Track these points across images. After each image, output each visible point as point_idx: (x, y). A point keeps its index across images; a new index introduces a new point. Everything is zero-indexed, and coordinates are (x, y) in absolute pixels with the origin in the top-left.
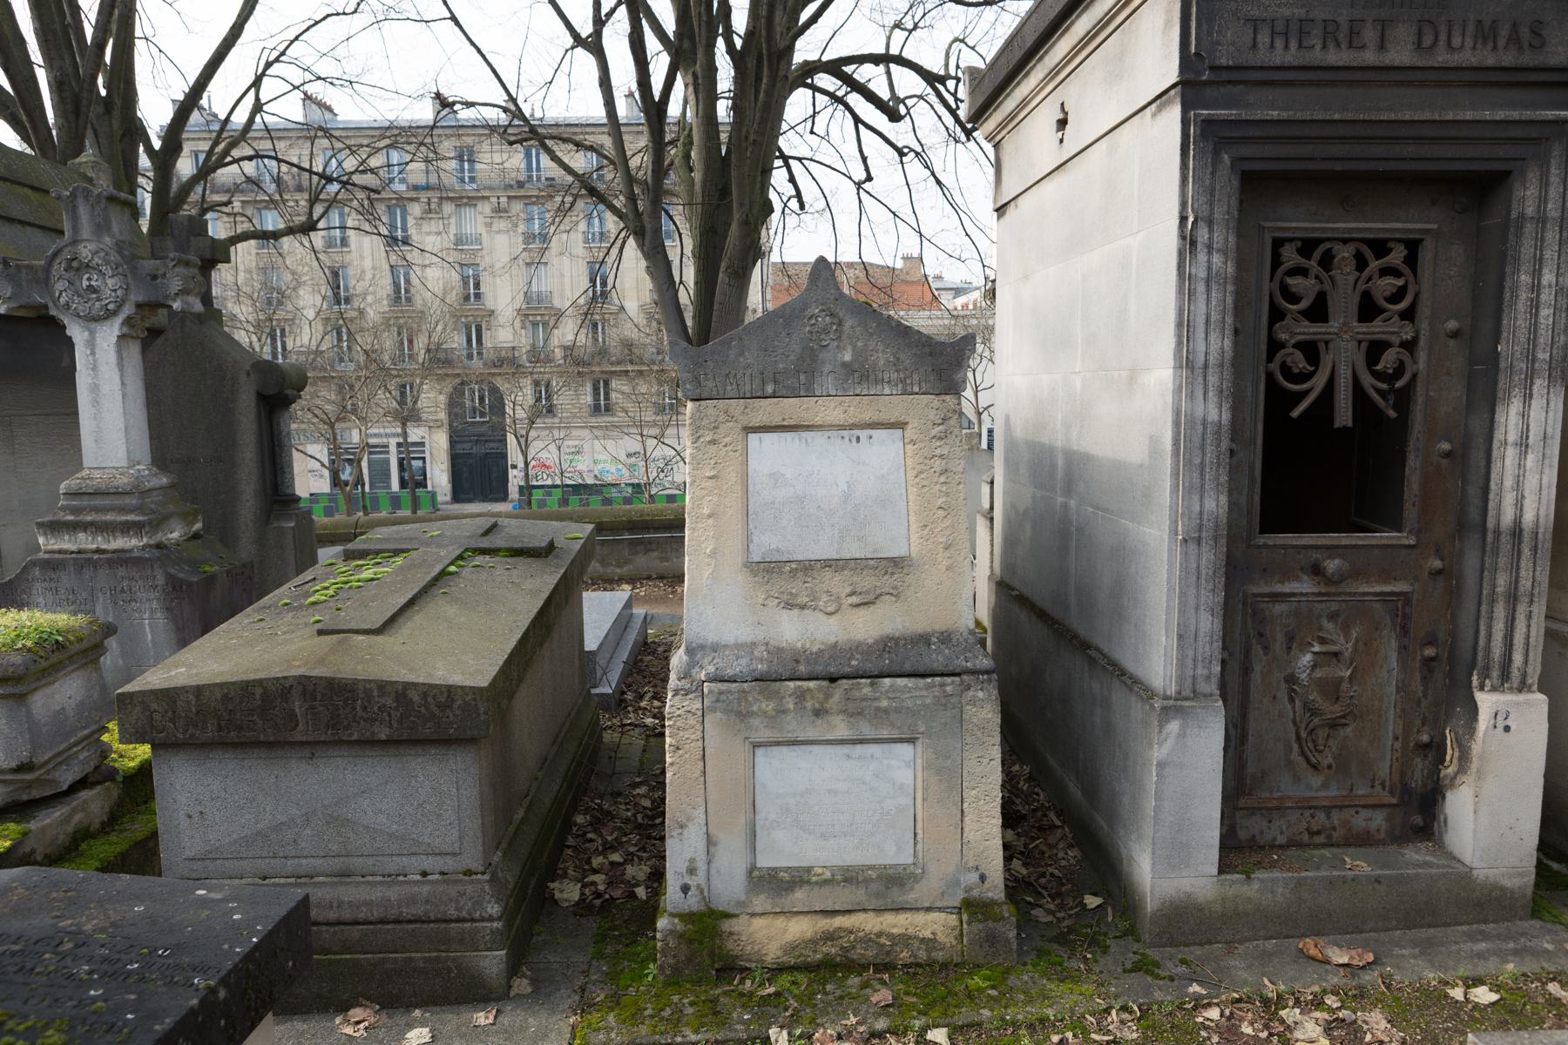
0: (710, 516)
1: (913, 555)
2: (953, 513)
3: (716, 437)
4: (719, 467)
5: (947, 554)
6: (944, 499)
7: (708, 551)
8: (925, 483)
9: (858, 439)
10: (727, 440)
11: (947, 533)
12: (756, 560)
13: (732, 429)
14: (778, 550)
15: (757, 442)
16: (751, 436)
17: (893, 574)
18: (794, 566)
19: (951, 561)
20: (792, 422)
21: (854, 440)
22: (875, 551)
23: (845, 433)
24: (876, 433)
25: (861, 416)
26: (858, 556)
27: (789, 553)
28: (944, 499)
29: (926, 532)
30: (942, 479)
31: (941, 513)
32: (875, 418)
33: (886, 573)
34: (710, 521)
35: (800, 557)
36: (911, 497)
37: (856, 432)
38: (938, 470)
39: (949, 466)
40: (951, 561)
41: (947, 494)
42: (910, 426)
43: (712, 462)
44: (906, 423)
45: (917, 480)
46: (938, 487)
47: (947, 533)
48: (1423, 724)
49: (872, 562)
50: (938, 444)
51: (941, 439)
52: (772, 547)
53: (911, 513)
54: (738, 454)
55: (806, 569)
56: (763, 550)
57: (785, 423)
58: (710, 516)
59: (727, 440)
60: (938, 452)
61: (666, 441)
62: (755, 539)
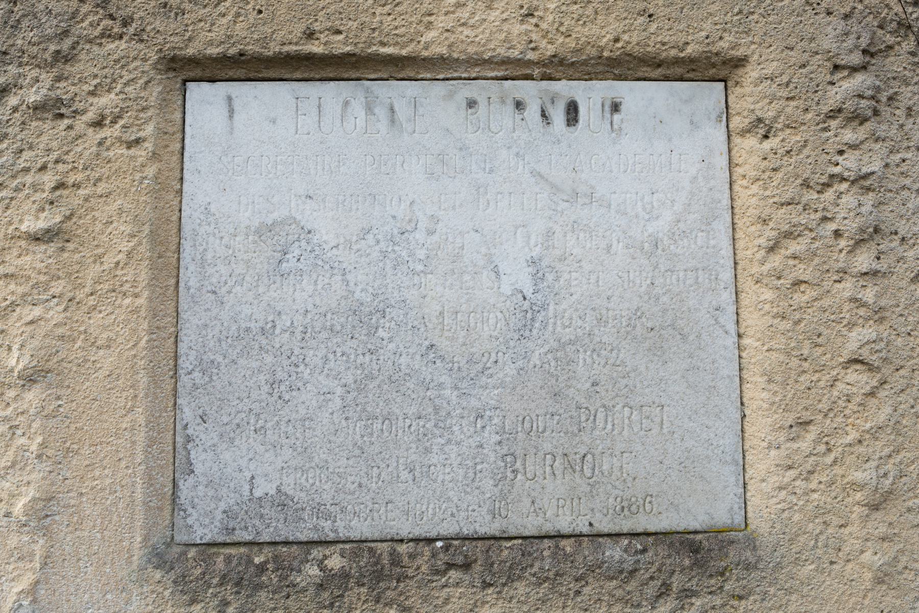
0: (29, 379)
1: (760, 523)
2: (898, 380)
3: (64, 90)
4: (75, 199)
5: (878, 525)
6: (868, 332)
7: (19, 507)
8: (803, 271)
9: (572, 112)
10: (106, 101)
11: (880, 448)
12: (205, 533)
13: (123, 62)
14: (282, 502)
15: (218, 112)
16: (196, 91)
17: (687, 594)
18: (335, 562)
19: (891, 550)
20: (339, 46)
21: (558, 115)
22: (626, 508)
23: (527, 90)
24: (629, 91)
25: (583, 32)
26: (564, 524)
27: (319, 511)
28: (868, 332)
29: (805, 444)
30: (864, 260)
31: (859, 380)
32: (633, 40)
33: (664, 591)
34: (33, 397)
35: (361, 528)
36: (753, 321)
37: (565, 88)
38: (852, 226)
39: (886, 213)
40: (891, 550)
41: (879, 314)
42: (751, 73)
43: (49, 179)
44: (740, 62)
45: (776, 261)
46: (847, 288)
47: (880, 448)
48: (117, 276)
49: (614, 552)
50: (848, 136)
51: (859, 119)
52: (264, 488)
53: (755, 377)
54: (141, 153)
55: (379, 576)
56: (229, 500)
57: (316, 48)
58: (29, 379)
59: (106, 101)
60: (850, 163)
61: (478, 421)
62: (201, 459)
